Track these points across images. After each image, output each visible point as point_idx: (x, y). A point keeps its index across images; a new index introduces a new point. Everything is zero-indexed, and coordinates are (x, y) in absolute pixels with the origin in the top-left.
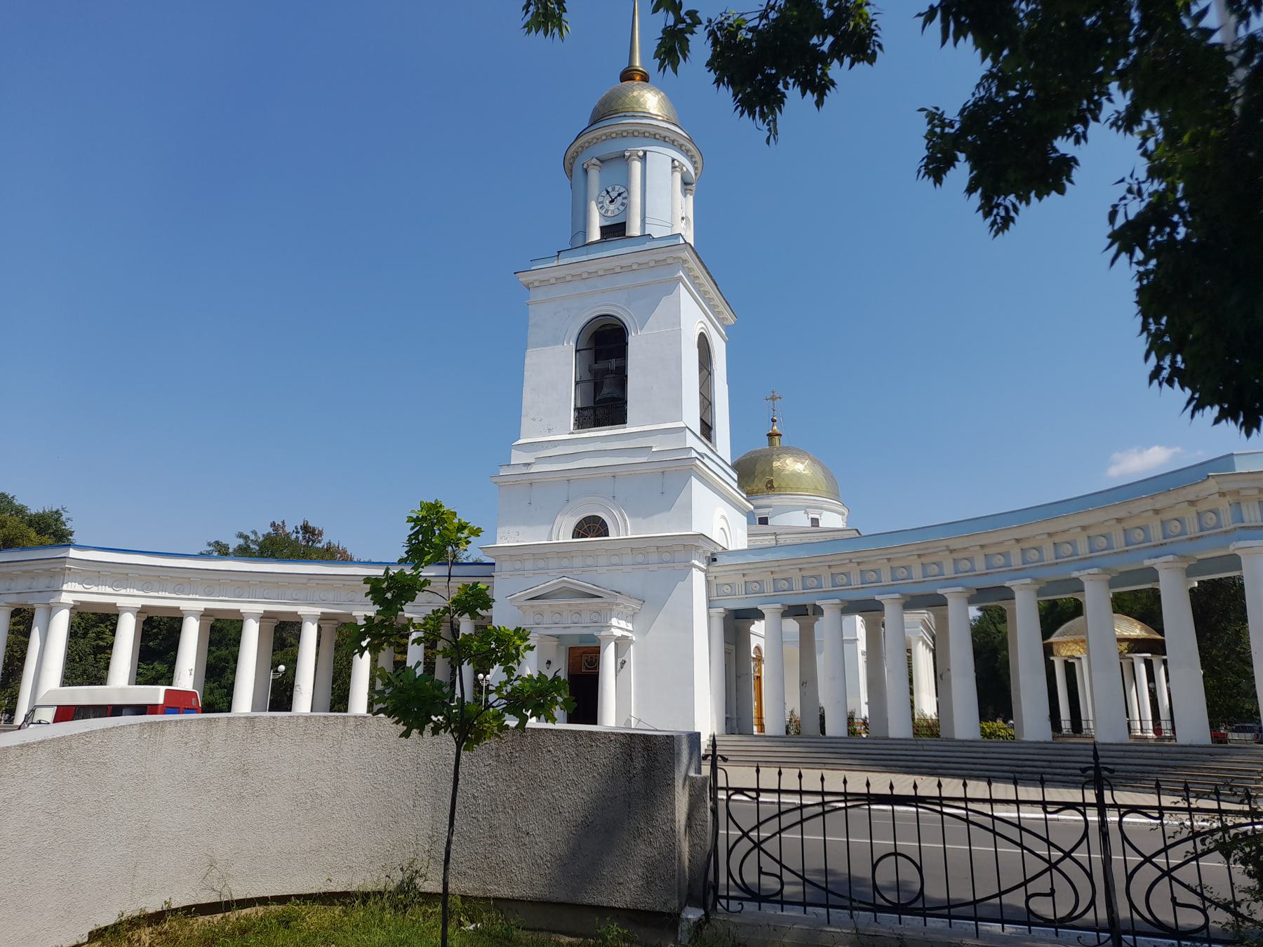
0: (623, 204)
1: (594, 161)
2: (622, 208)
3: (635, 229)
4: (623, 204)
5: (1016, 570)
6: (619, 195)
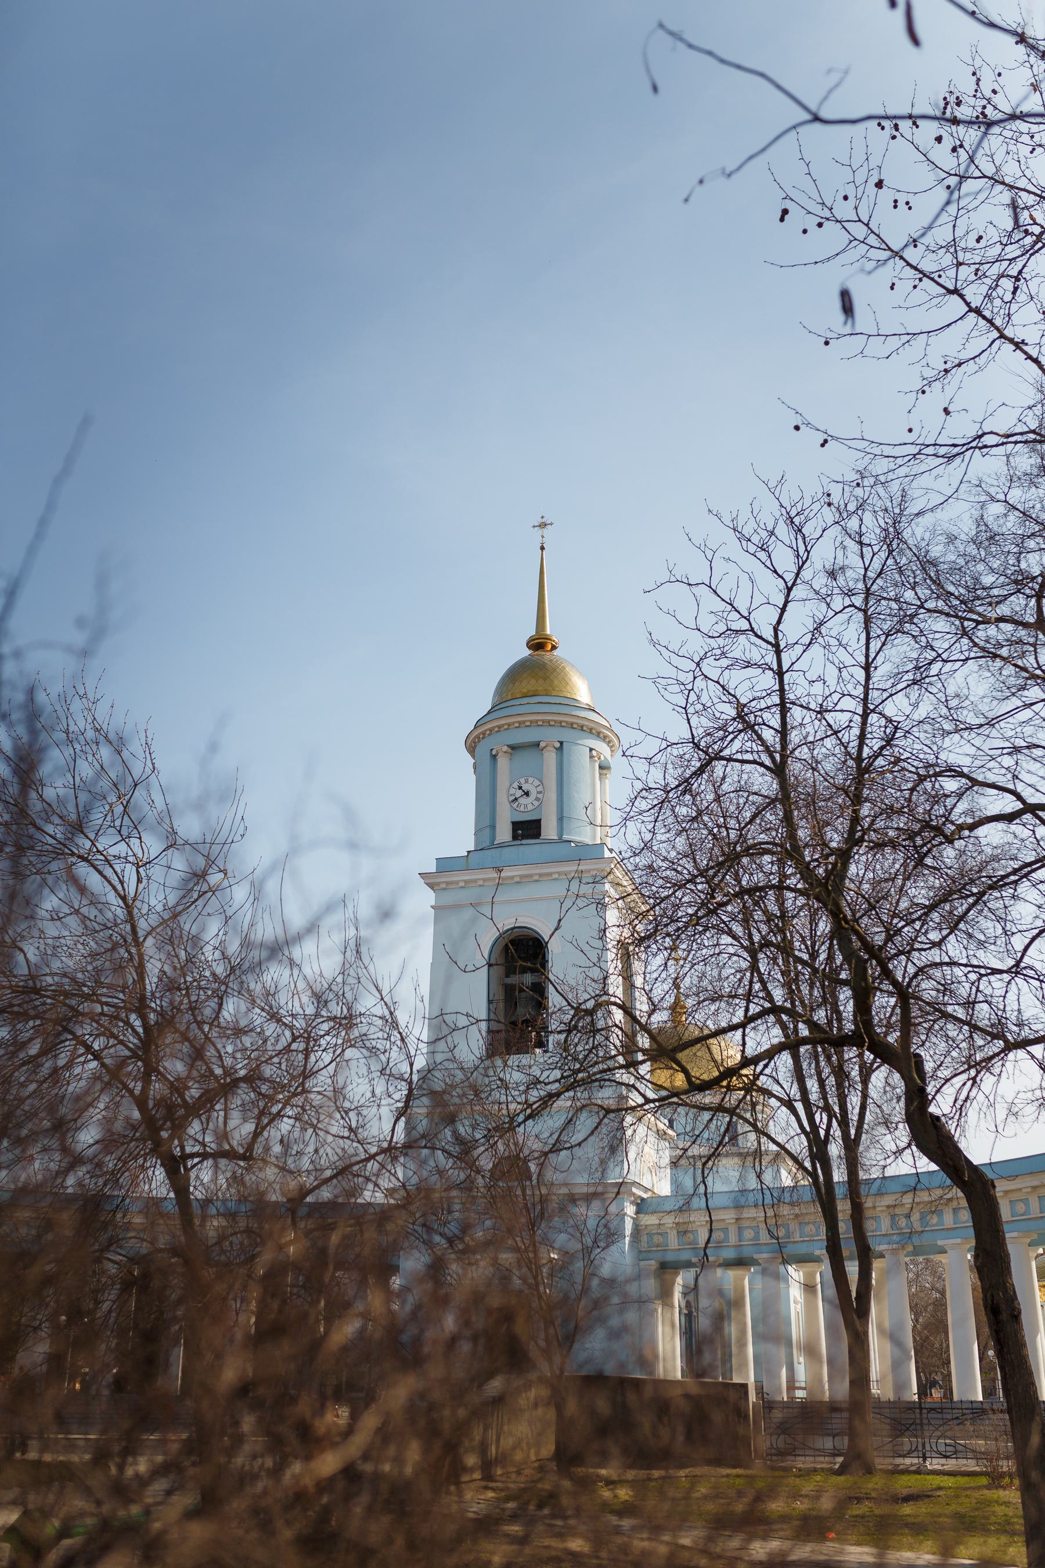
0: (537, 799)
1: (505, 748)
2: (536, 803)
3: (549, 831)
4: (537, 799)
5: (948, 1229)
6: (520, 788)
